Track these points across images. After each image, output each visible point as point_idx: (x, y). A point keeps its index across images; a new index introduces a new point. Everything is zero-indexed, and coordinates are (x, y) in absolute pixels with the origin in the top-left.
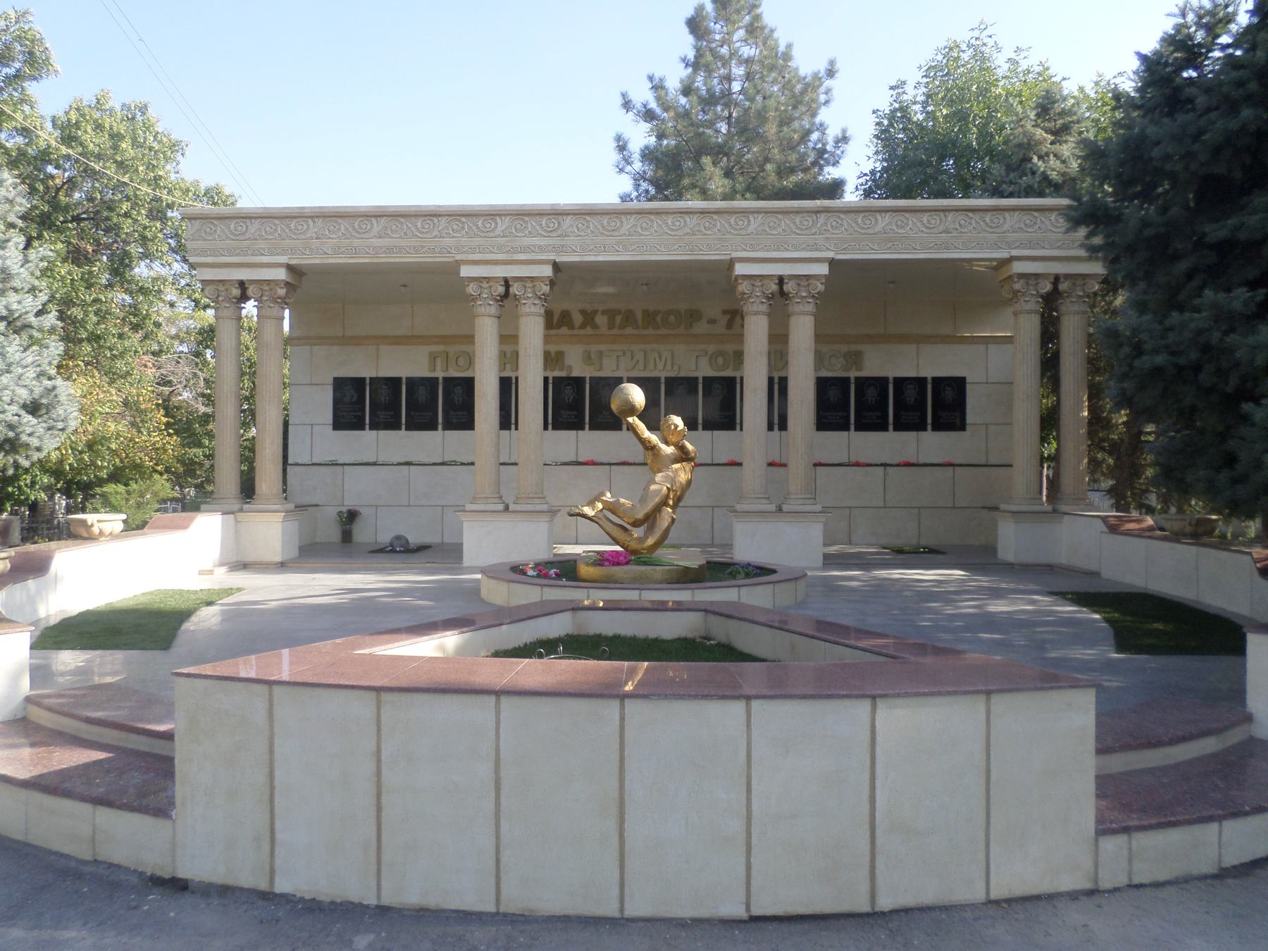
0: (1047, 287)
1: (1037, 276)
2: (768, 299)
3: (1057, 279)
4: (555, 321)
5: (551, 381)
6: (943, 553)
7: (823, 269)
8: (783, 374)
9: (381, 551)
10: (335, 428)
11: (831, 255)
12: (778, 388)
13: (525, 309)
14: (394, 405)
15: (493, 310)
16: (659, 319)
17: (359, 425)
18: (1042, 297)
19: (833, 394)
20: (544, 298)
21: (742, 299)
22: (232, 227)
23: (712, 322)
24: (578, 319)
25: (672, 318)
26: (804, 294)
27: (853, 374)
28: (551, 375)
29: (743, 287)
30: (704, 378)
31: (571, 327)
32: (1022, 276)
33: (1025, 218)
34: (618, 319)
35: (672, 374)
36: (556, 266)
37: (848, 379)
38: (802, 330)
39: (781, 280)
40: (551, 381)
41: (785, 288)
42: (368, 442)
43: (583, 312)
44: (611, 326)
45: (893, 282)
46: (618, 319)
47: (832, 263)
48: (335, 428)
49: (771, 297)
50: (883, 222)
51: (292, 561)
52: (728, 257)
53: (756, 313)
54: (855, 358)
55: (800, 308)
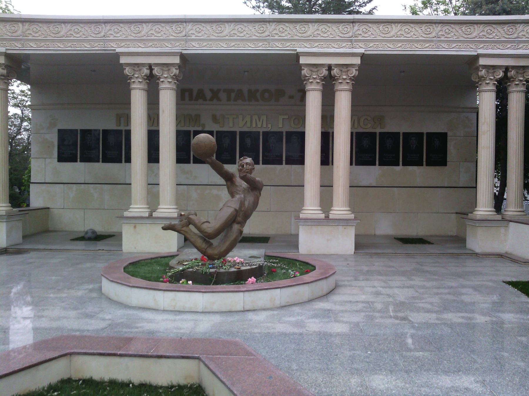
0: (501, 74)
1: (494, 67)
2: (322, 80)
3: (507, 69)
4: (184, 95)
5: (354, 135)
6: (429, 243)
7: (357, 61)
8: (127, 128)
9: (82, 239)
10: (58, 161)
11: (362, 51)
12: (153, 138)
13: (484, 87)
14: (85, 147)
15: (143, 86)
16: (258, 95)
17: (73, 159)
18: (497, 81)
19: (366, 143)
20: (175, 77)
21: (305, 80)
22: (93, 29)
23: (291, 97)
24: (208, 95)
25: (266, 95)
26: (344, 77)
27: (378, 130)
28: (355, 131)
29: (305, 72)
30: (286, 132)
31: (205, 99)
32: (485, 67)
33: (280, 26)
34: (233, 95)
35: (246, 129)
36: (183, 57)
37: (375, 133)
38: (343, 102)
39: (330, 68)
40: (354, 135)
41: (509, 74)
42: (78, 170)
43: (211, 90)
44: (229, 99)
45: (404, 72)
46: (233, 95)
47: (363, 56)
48: (58, 161)
49: (324, 79)
50: (476, 32)
51: (183, 247)
52: (475, 54)
53: (313, 90)
54: (380, 120)
55: (313, 87)
